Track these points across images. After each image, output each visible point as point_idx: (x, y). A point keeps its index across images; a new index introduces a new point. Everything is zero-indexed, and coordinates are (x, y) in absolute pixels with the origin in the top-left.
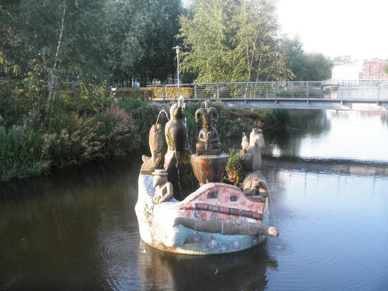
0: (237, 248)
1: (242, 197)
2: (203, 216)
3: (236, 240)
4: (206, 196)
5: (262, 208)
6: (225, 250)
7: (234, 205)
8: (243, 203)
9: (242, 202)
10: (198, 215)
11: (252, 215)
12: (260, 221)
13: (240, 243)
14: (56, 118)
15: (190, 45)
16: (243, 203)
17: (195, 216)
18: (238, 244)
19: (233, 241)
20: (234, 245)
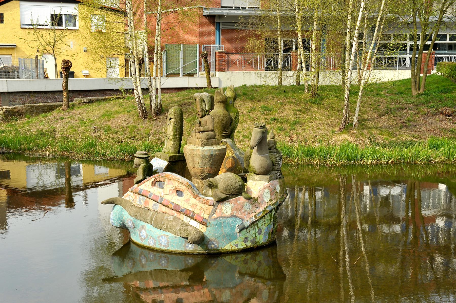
0: (164, 246)
1: (187, 194)
2: (146, 203)
3: (163, 237)
4: (150, 184)
5: (208, 212)
6: (163, 259)
7: (178, 200)
8: (188, 200)
9: (186, 199)
10: (142, 202)
11: (193, 216)
12: (204, 226)
13: (168, 242)
14: (257, 263)
15: (73, 73)
16: (188, 200)
17: (140, 201)
18: (166, 242)
19: (160, 236)
20: (161, 242)
